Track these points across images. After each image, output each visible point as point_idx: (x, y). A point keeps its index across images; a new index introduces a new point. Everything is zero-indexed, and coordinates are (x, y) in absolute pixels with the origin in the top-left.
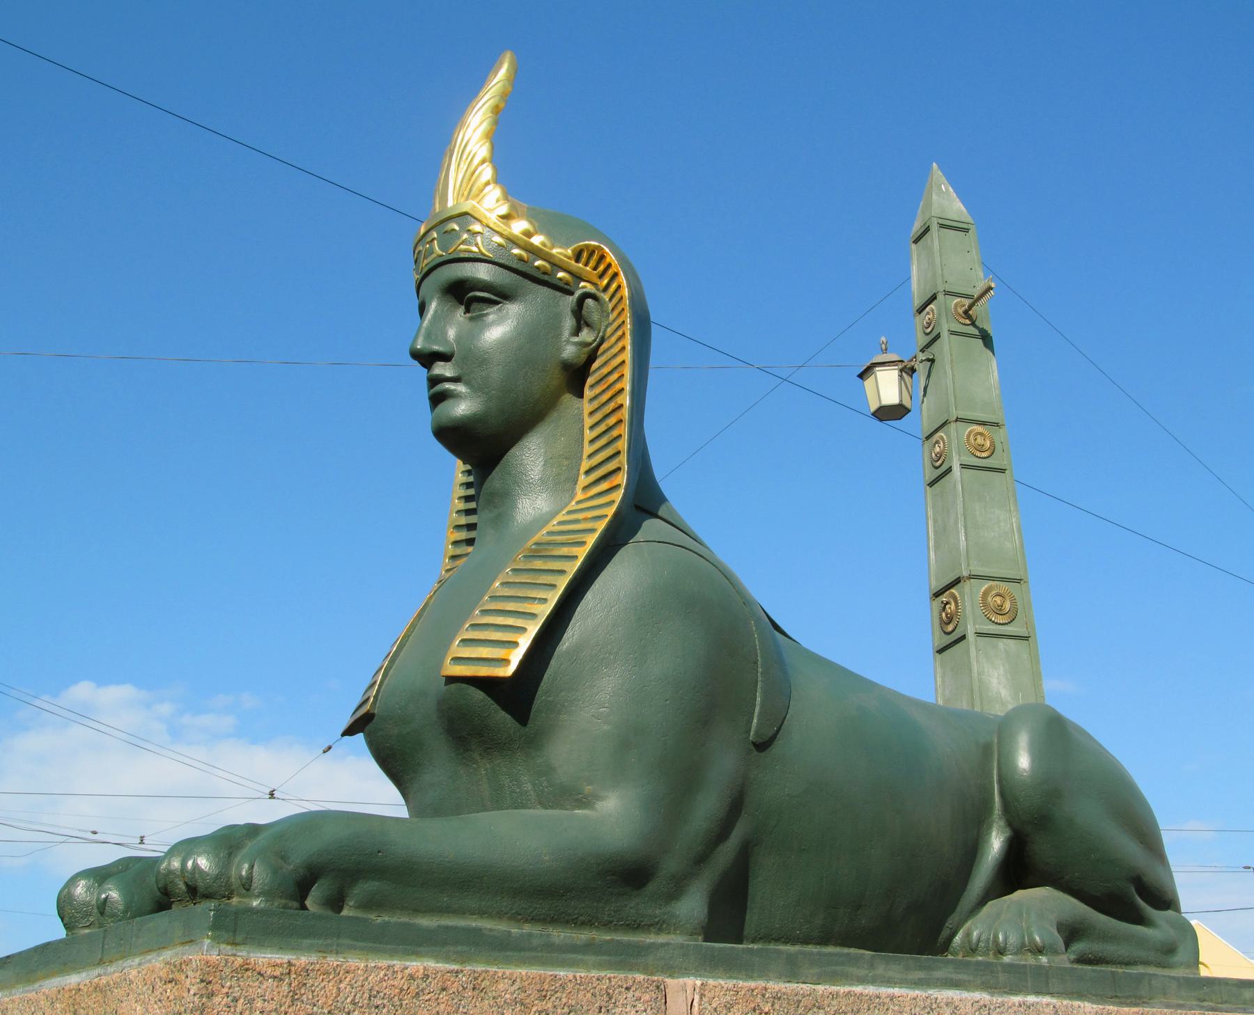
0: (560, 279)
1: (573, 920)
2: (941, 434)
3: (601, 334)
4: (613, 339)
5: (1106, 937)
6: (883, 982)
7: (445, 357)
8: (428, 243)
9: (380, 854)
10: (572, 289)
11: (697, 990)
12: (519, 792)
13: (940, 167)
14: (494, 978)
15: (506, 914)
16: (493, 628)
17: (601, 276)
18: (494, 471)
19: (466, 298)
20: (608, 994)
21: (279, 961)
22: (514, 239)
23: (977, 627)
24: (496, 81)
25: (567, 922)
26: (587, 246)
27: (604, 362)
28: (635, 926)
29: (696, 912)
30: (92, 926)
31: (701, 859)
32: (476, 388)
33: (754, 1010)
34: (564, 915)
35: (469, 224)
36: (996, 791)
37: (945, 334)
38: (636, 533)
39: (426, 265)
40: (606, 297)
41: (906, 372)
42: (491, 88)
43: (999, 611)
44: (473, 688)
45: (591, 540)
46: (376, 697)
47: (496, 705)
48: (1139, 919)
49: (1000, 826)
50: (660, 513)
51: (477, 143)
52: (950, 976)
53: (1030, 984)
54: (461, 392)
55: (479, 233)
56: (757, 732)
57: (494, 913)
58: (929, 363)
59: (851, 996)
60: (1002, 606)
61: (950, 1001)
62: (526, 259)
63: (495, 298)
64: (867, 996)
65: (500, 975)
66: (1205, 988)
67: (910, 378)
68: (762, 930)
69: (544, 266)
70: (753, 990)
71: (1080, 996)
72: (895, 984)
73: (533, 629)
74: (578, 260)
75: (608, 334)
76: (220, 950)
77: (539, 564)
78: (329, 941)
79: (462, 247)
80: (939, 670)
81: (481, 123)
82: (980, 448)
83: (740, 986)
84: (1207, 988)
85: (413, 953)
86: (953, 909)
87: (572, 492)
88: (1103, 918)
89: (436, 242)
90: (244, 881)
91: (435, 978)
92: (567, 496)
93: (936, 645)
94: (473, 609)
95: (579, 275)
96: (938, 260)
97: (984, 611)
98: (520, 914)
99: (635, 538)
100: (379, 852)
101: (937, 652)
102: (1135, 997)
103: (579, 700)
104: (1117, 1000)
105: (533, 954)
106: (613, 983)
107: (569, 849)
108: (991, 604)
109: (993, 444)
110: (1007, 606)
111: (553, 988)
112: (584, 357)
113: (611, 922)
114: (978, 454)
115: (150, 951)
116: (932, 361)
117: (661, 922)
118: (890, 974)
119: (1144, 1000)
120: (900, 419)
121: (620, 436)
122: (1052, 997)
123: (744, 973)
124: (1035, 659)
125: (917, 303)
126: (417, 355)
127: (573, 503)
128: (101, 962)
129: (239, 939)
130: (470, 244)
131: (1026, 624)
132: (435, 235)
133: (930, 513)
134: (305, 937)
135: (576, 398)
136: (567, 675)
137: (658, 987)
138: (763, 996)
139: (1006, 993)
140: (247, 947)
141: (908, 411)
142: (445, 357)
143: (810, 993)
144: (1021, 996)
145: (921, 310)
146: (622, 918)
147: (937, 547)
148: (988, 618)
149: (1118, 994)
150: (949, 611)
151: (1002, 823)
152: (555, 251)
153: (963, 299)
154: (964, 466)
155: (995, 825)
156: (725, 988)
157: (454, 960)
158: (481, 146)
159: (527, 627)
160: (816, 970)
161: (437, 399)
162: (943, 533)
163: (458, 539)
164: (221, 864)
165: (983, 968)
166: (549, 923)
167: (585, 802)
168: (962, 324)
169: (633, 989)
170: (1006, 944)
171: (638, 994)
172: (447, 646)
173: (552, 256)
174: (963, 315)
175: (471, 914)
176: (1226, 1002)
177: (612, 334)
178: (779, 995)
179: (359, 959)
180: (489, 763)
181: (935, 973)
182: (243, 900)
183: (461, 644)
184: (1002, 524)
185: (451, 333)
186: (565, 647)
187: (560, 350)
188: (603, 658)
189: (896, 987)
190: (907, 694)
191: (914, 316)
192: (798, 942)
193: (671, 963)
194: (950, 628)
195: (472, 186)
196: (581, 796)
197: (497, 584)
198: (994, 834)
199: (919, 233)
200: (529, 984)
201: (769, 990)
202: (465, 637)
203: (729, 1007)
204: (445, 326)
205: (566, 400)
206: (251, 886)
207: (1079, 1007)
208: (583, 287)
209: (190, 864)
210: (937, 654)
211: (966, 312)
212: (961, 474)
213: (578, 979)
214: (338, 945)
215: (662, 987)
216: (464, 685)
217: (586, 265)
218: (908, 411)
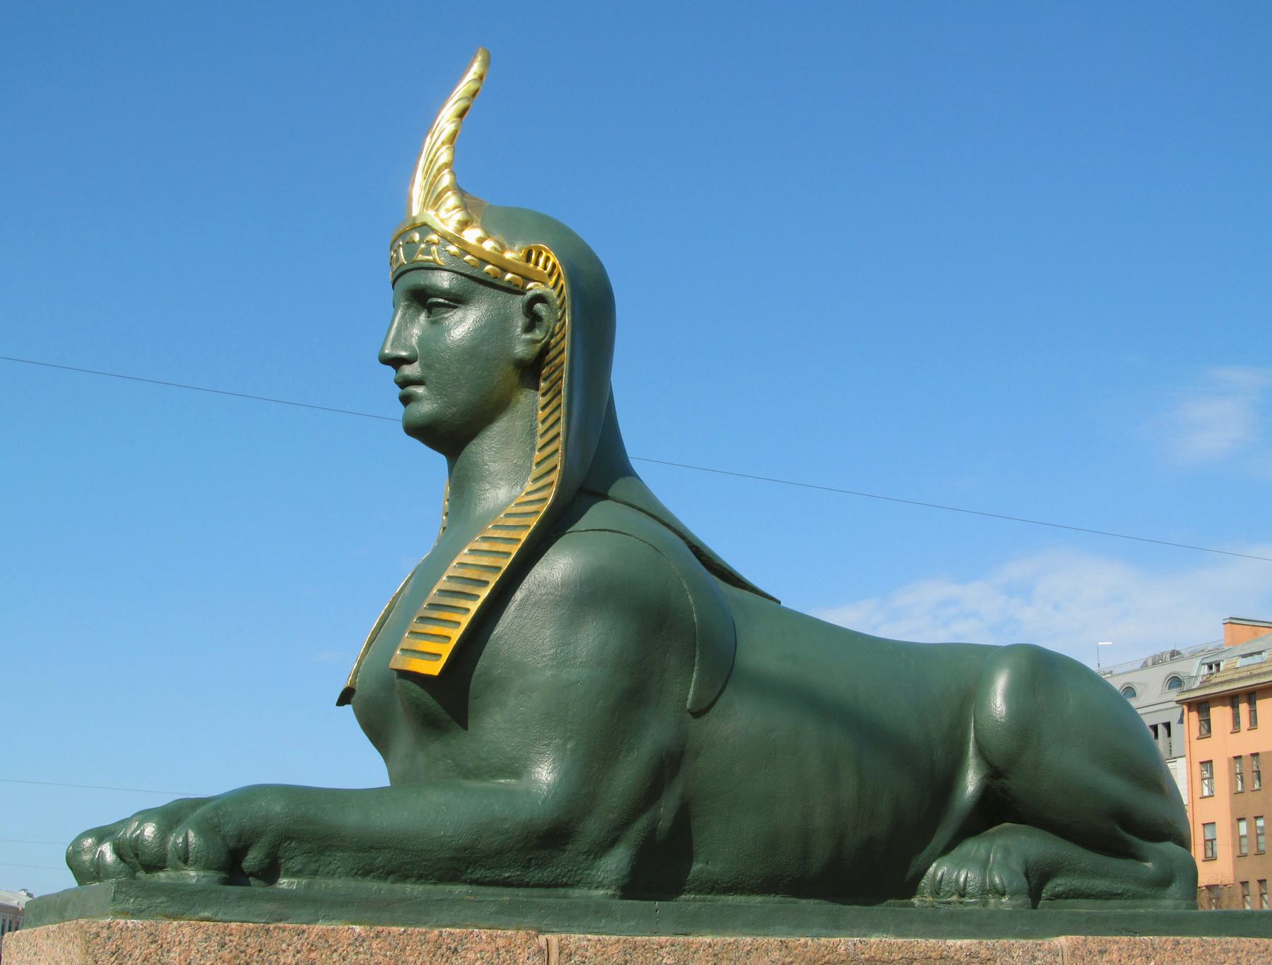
0: (509, 282)
17: (551, 275)
26: (536, 248)
36: (971, 739)
56: (693, 702)
71: (1121, 934)
89: (401, 249)
99: (576, 525)
132: (401, 243)
161: (406, 400)
185: (416, 331)
190: (379, 754)
197: (435, 591)
208: (531, 289)
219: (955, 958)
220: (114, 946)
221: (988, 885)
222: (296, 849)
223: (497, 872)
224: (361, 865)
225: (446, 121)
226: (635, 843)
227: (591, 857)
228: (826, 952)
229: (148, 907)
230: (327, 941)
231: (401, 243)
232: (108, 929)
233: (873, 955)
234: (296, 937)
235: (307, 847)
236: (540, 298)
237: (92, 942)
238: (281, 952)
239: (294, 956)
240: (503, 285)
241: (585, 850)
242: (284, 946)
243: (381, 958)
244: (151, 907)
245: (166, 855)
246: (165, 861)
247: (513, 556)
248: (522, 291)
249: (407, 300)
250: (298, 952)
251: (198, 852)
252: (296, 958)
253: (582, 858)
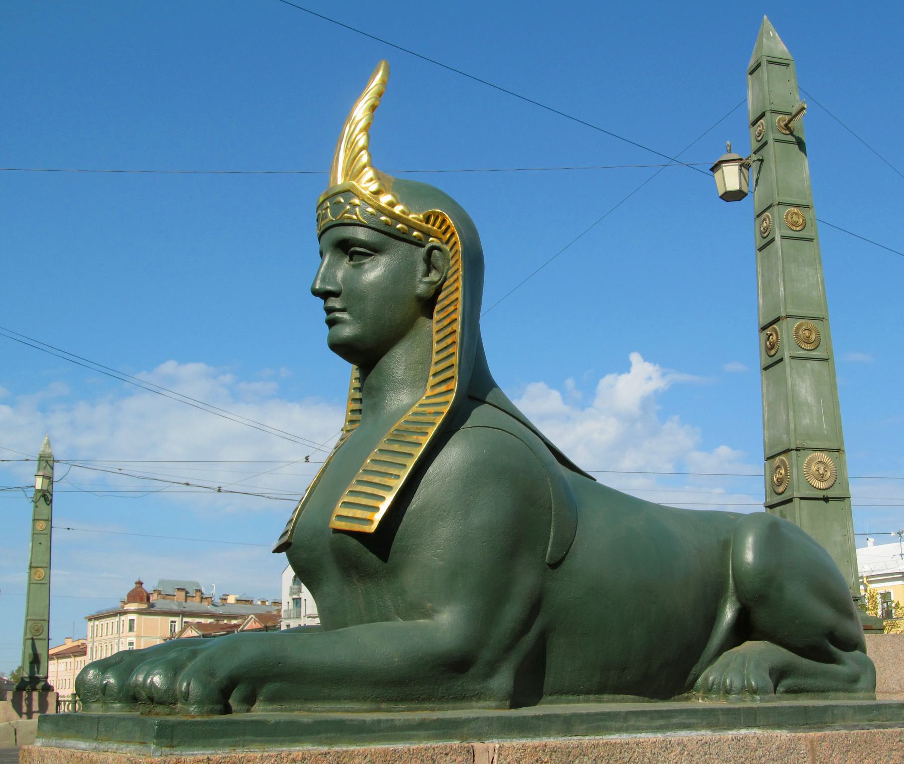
1: (416, 698)
2: (767, 213)
3: (444, 275)
4: (452, 280)
5: (806, 675)
6: (633, 730)
7: (336, 294)
8: (324, 209)
9: (280, 665)
10: (424, 243)
11: (496, 751)
12: (383, 606)
13: (769, 19)
14: (352, 756)
15: (368, 698)
16: (363, 495)
17: (444, 233)
18: (372, 372)
20: (433, 759)
21: (201, 758)
22: (382, 210)
23: (791, 352)
24: (371, 87)
25: (412, 700)
26: (434, 213)
27: (445, 296)
28: (461, 698)
29: (504, 685)
30: (98, 701)
31: (508, 649)
32: (358, 317)
33: (537, 761)
34: (409, 696)
35: (351, 198)
37: (771, 142)
38: (466, 421)
39: (323, 226)
40: (448, 248)
41: (744, 167)
42: (369, 91)
43: (807, 341)
44: (350, 538)
45: (432, 431)
46: (292, 531)
47: (366, 549)
48: (831, 659)
49: (733, 600)
50: (487, 400)
52: (683, 721)
53: (742, 721)
54: (346, 320)
55: (357, 205)
56: (550, 557)
57: (360, 698)
58: (760, 162)
59: (608, 745)
60: (809, 337)
61: (681, 741)
62: (390, 224)
63: (369, 252)
64: (619, 744)
65: (356, 753)
66: (874, 711)
67: (747, 171)
68: (557, 687)
69: (403, 228)
70: (536, 748)
71: (780, 726)
72: (643, 730)
73: (390, 498)
74: (427, 221)
75: (449, 275)
76: (162, 752)
77: (396, 447)
78: (237, 739)
79: (346, 215)
80: (765, 382)
82: (795, 224)
83: (527, 746)
84: (876, 711)
85: (296, 741)
86: (696, 661)
87: (425, 388)
88: (805, 661)
89: (329, 210)
90: (184, 695)
91: (310, 760)
92: (421, 391)
93: (763, 364)
94: (352, 479)
95: (428, 233)
96: (766, 88)
97: (796, 341)
98: (378, 698)
100: (279, 663)
101: (764, 369)
102: (821, 723)
103: (423, 544)
104: (808, 726)
105: (382, 734)
106: (436, 752)
107: (413, 653)
108: (802, 336)
109: (804, 221)
110: (813, 337)
111: (394, 758)
112: (432, 292)
113: (443, 697)
114: (794, 228)
115: (123, 741)
116: (762, 161)
117: (480, 693)
118: (639, 724)
119: (828, 724)
120: (740, 200)
121: (453, 354)
122: (758, 728)
123: (533, 733)
124: (832, 375)
125: (752, 118)
126: (316, 293)
127: (424, 398)
128: (96, 739)
129: (175, 743)
130: (351, 213)
131: (827, 349)
132: (329, 205)
133: (759, 270)
134: (223, 737)
135: (428, 319)
136: (415, 527)
137: (468, 751)
138: (544, 751)
139: (725, 729)
140: (181, 748)
141: (746, 195)
142: (336, 294)
143: (578, 746)
144: (736, 730)
145: (754, 123)
146: (452, 693)
147: (764, 294)
148: (799, 346)
149: (809, 722)
150: (772, 341)
151: (734, 599)
152: (411, 217)
153: (784, 116)
154: (783, 237)
155: (729, 599)
156: (516, 748)
157: (325, 743)
160: (585, 726)
161: (331, 323)
162: (768, 286)
163: (355, 409)
164: (169, 682)
165: (708, 713)
166: (399, 701)
167: (427, 614)
168: (784, 134)
169: (451, 754)
170: (731, 687)
171: (454, 757)
172: (348, 482)
173: (408, 220)
174: (784, 127)
175: (345, 700)
176: (890, 720)
177: (452, 275)
178: (555, 749)
179: (259, 748)
180: (363, 585)
181: (673, 720)
182: (185, 706)
183: (343, 505)
184: (810, 278)
185: (340, 275)
186: (413, 507)
187: (415, 287)
188: (439, 515)
189: (643, 732)
191: (750, 127)
192: (582, 694)
193: (480, 731)
194: (772, 352)
195: (354, 169)
196: (424, 610)
197: (368, 461)
198: (728, 606)
199: (754, 67)
200: (376, 758)
201: (548, 747)
202: (346, 501)
203: (518, 761)
204: (335, 271)
205: (420, 322)
206: (188, 698)
207: (777, 736)
208: (432, 241)
209: (149, 681)
210: (764, 371)
211: (786, 125)
212: (781, 242)
213: (411, 750)
214: (244, 741)
215: (472, 751)
216: (344, 535)
217: (434, 225)
218: (746, 195)
225: (360, 112)
247: (424, 446)
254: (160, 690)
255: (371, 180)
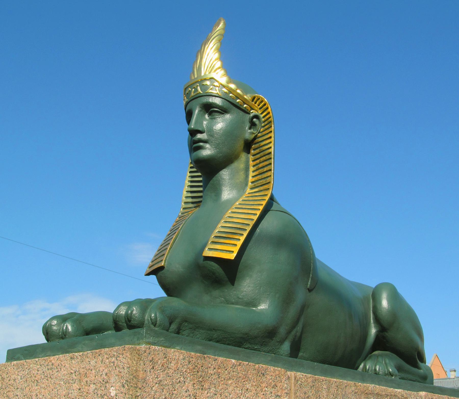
0: (238, 103)
19: (211, 110)
51: (213, 52)
56: (310, 285)
81: (215, 45)
132: (198, 85)
142: (201, 132)
158: (214, 54)
159: (243, 234)
208: (252, 112)
219: (398, 396)
220: (151, 358)
221: (386, 372)
222: (187, 326)
223: (253, 346)
224: (208, 337)
226: (291, 340)
227: (280, 344)
228: (366, 389)
229: (158, 342)
230: (224, 365)
231: (198, 85)
232: (149, 349)
233: (378, 392)
234: (214, 362)
235: (191, 326)
236: (256, 117)
237: (143, 355)
238: (209, 368)
239: (213, 370)
240: (243, 108)
241: (279, 341)
242: (210, 365)
243: (241, 375)
244: (159, 342)
245: (144, 321)
246: (143, 324)
248: (249, 112)
249: (201, 108)
250: (215, 369)
251: (161, 322)
252: (214, 371)
253: (277, 344)
254: (285, 368)
255: (219, 68)
